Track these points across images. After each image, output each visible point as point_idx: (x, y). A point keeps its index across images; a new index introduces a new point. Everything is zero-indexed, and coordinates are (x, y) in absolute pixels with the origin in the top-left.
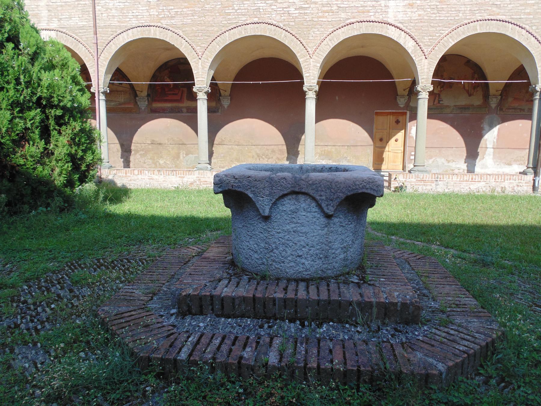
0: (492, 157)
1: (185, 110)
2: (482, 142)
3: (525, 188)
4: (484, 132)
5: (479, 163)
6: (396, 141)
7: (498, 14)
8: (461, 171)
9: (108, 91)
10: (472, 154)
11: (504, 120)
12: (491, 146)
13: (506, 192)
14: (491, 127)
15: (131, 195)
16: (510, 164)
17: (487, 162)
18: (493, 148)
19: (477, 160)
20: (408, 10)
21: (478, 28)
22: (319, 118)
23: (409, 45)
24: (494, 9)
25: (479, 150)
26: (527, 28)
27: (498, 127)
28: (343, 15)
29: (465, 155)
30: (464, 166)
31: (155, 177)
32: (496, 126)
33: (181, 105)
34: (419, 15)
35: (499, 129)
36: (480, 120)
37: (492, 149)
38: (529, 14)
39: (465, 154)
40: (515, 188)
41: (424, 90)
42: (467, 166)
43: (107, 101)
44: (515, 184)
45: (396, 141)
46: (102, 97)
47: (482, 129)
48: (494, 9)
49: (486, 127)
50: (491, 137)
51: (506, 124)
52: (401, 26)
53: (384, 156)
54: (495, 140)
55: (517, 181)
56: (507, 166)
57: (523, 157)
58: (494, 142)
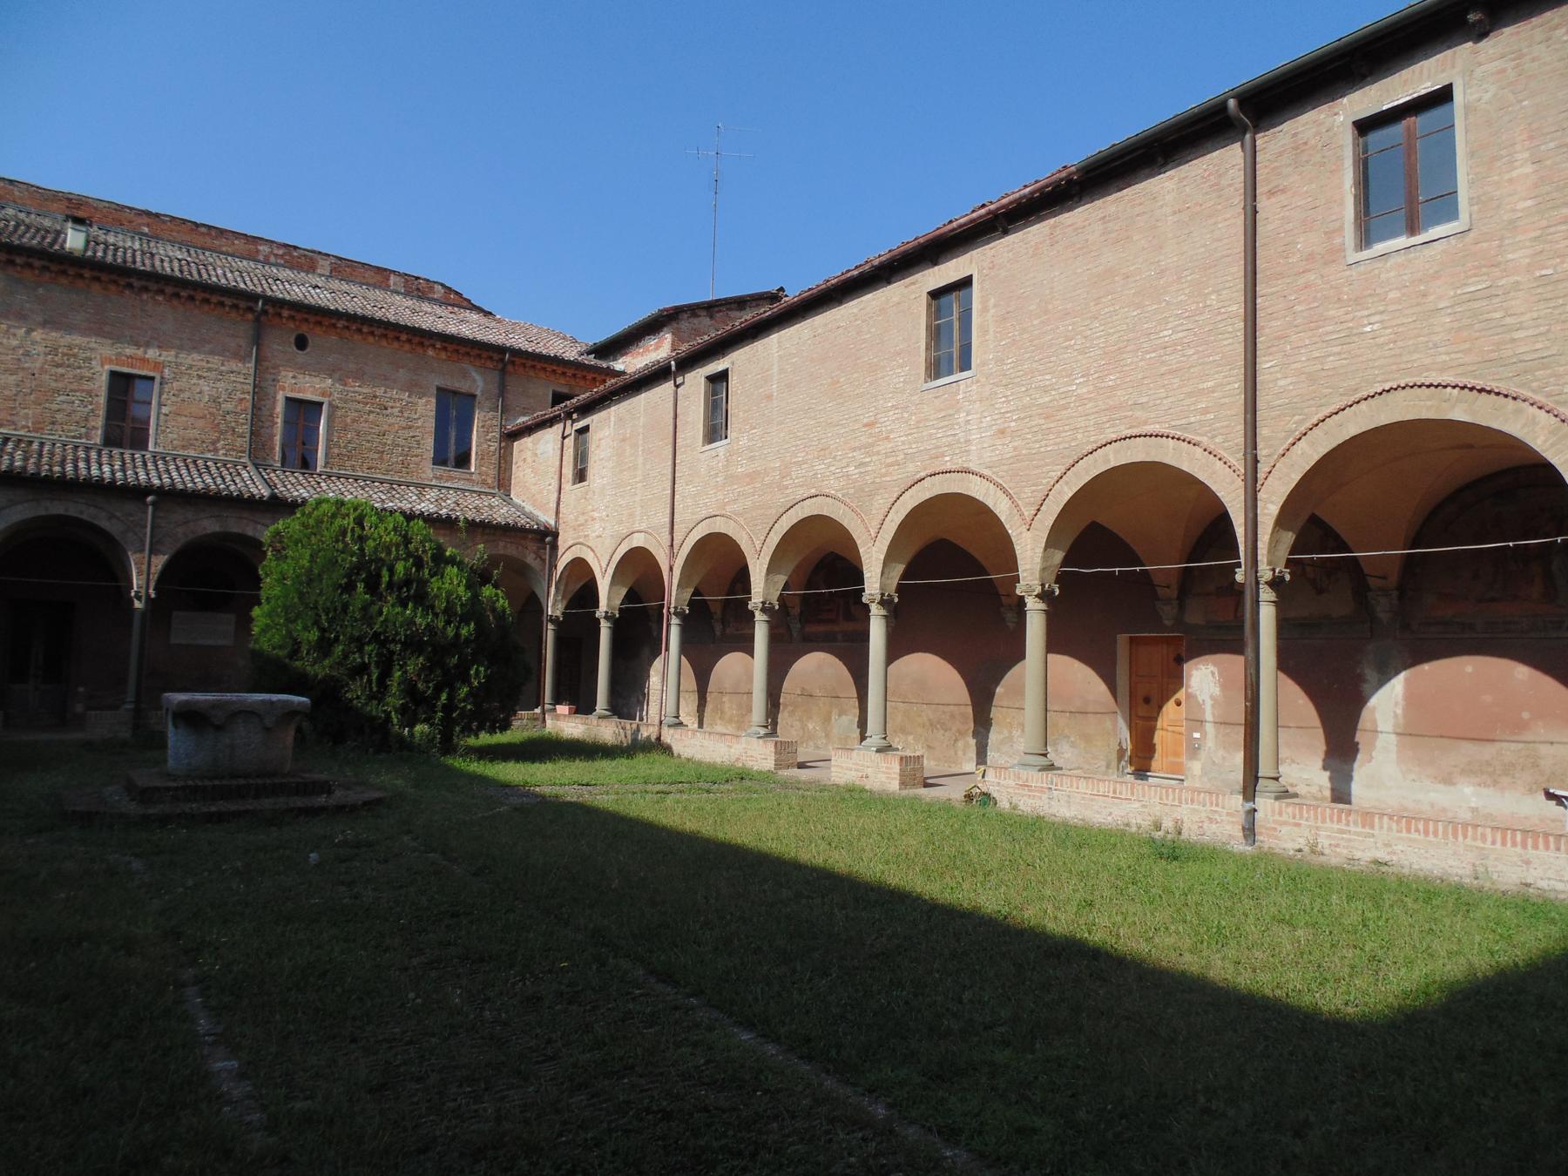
0: (1393, 756)
1: (840, 637)
2: (1365, 713)
3: (1228, 827)
4: (1366, 687)
5: (1362, 774)
6: (1178, 704)
7: (1145, 423)
8: (1314, 790)
9: (1288, 577)
10: (1342, 748)
11: (1419, 655)
12: (1390, 729)
13: (1185, 836)
14: (1385, 676)
15: (1168, 824)
16: (1448, 780)
17: (1382, 766)
18: (1398, 734)
19: (1356, 765)
20: (999, 442)
21: (1111, 457)
22: (893, 654)
23: (1001, 507)
24: (1138, 414)
25: (1359, 737)
26: (1204, 440)
27: (1402, 676)
28: (911, 467)
29: (1324, 748)
30: (1322, 779)
31: (706, 743)
32: (1397, 673)
33: (837, 628)
34: (1015, 448)
35: (1407, 680)
36: (1180, 661)
37: (1393, 737)
38: (1205, 411)
39: (1321, 746)
40: (1206, 825)
41: (1029, 592)
42: (1331, 779)
43: (1279, 605)
44: (1204, 815)
45: (1178, 704)
46: (1266, 594)
47: (1360, 679)
48: (1138, 414)
49: (1370, 674)
50: (1388, 703)
51: (1426, 667)
52: (986, 472)
53: (1157, 740)
54: (1399, 711)
55: (1208, 807)
56: (1441, 787)
57: (1488, 764)
58: (1396, 715)
